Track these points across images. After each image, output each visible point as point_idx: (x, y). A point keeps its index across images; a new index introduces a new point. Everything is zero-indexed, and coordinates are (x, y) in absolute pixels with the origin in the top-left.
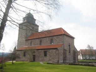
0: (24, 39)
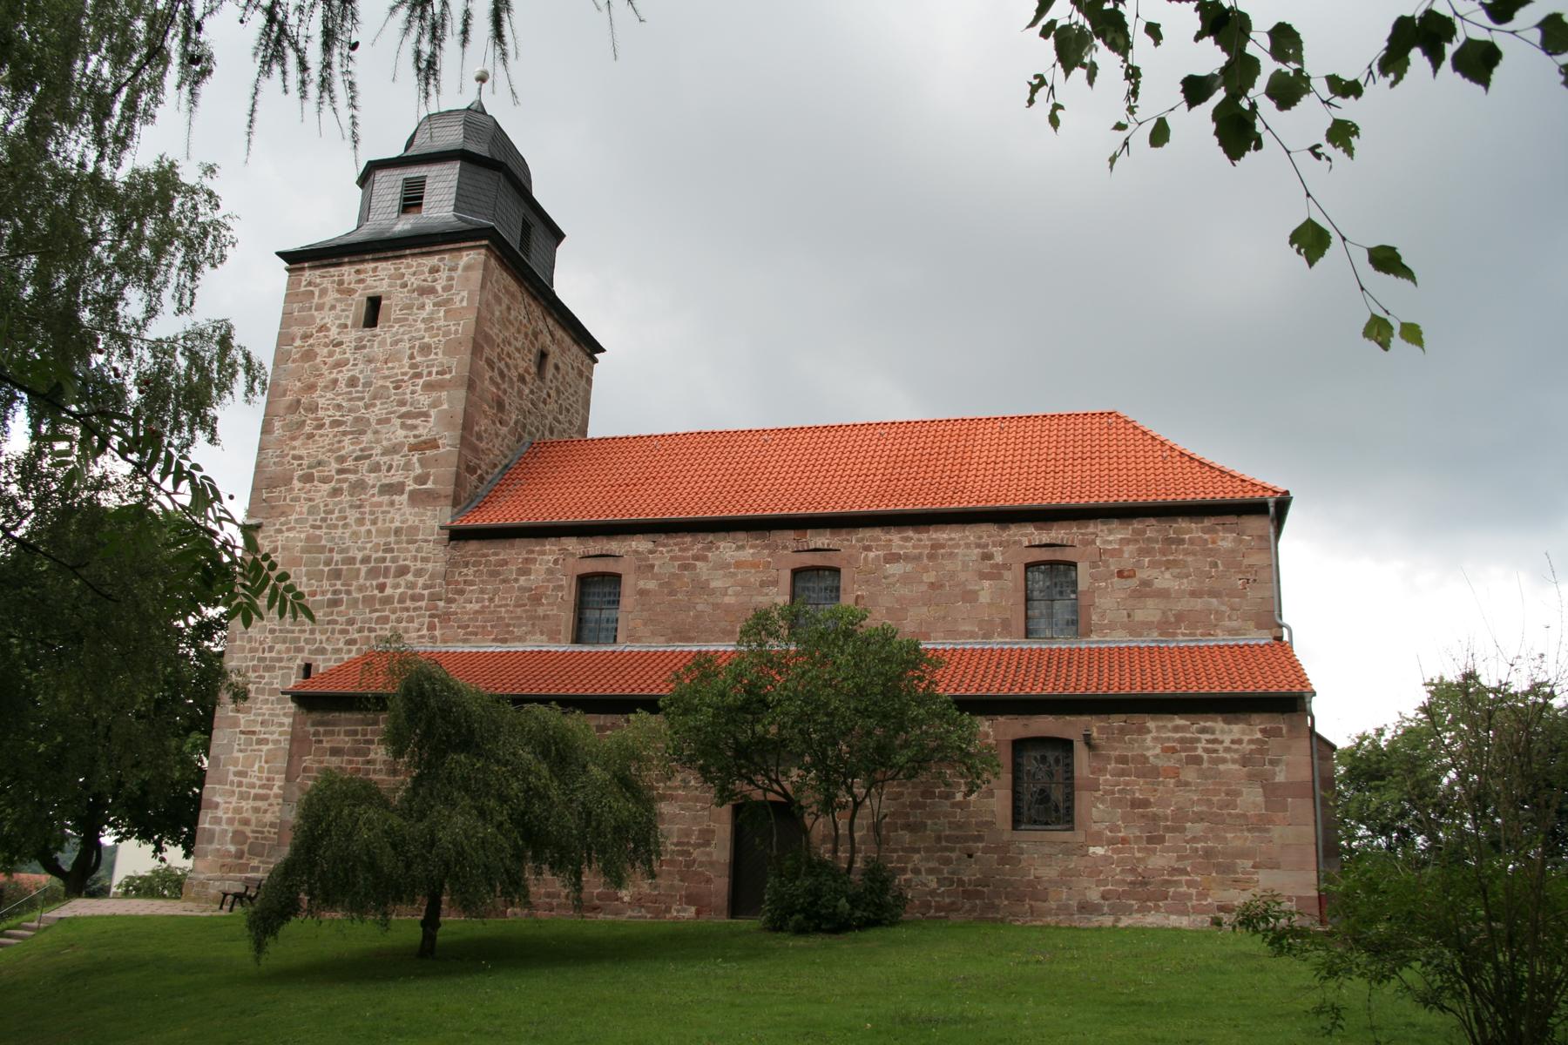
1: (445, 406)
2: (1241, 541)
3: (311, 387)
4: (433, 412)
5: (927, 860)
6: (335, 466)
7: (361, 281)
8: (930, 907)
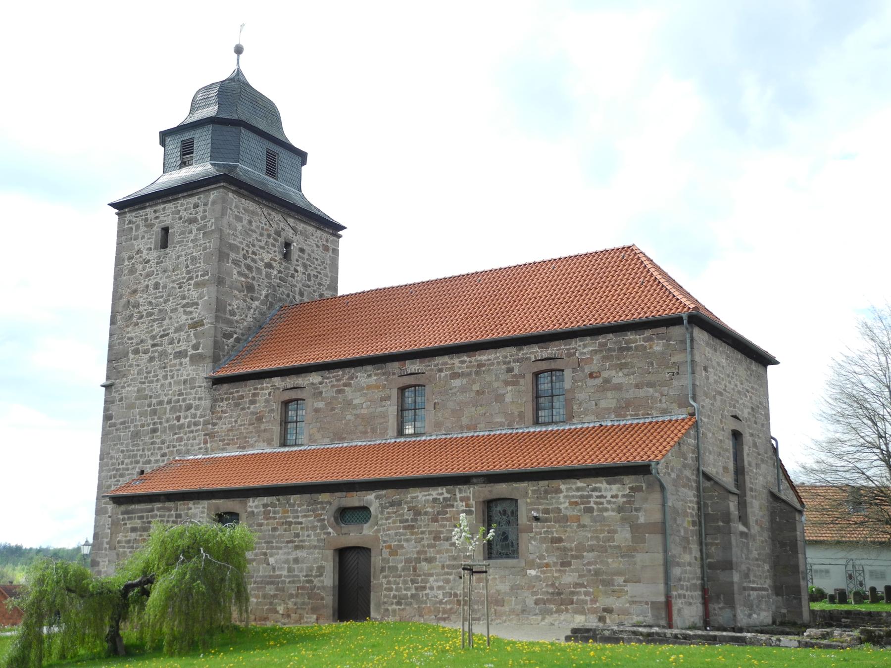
0: (204, 372)
1: (206, 298)
2: (669, 345)
3: (135, 292)
4: (200, 302)
5: (437, 581)
6: (150, 342)
7: (157, 218)
8: (439, 611)
